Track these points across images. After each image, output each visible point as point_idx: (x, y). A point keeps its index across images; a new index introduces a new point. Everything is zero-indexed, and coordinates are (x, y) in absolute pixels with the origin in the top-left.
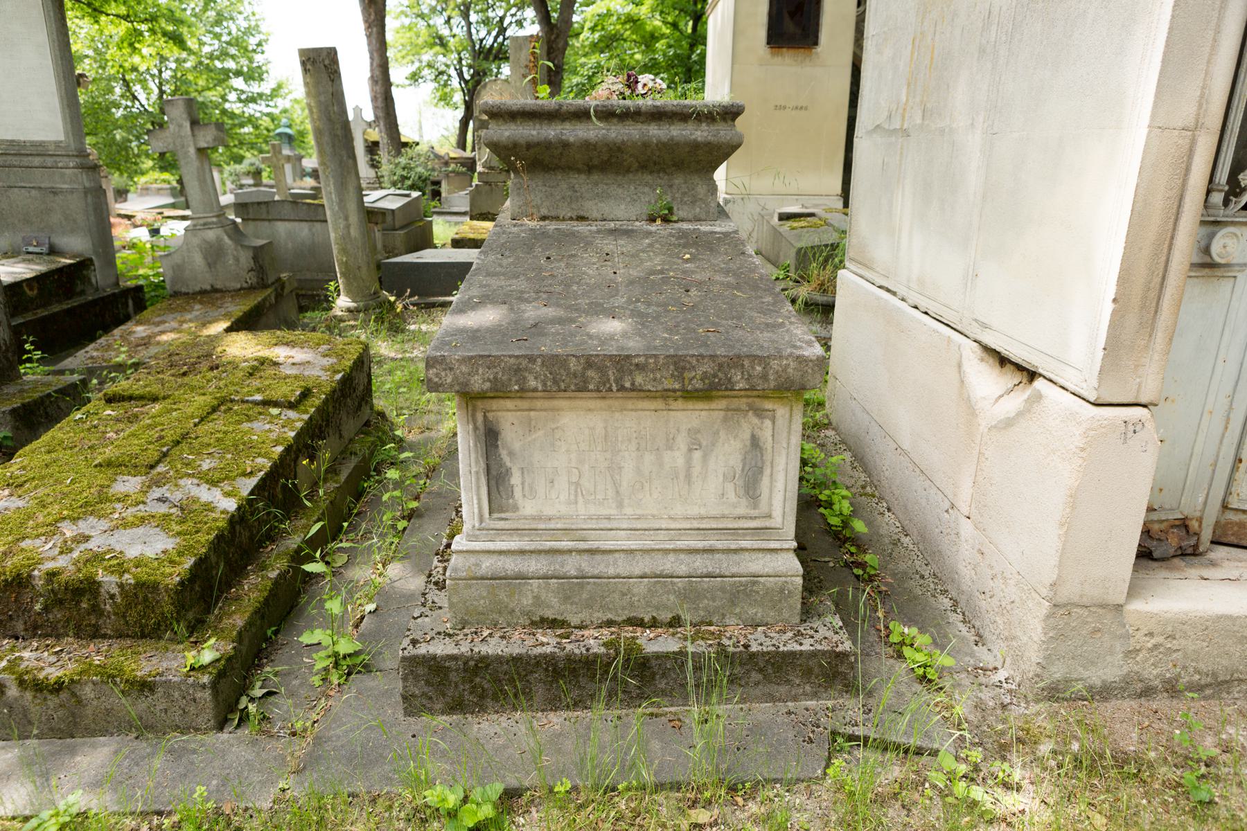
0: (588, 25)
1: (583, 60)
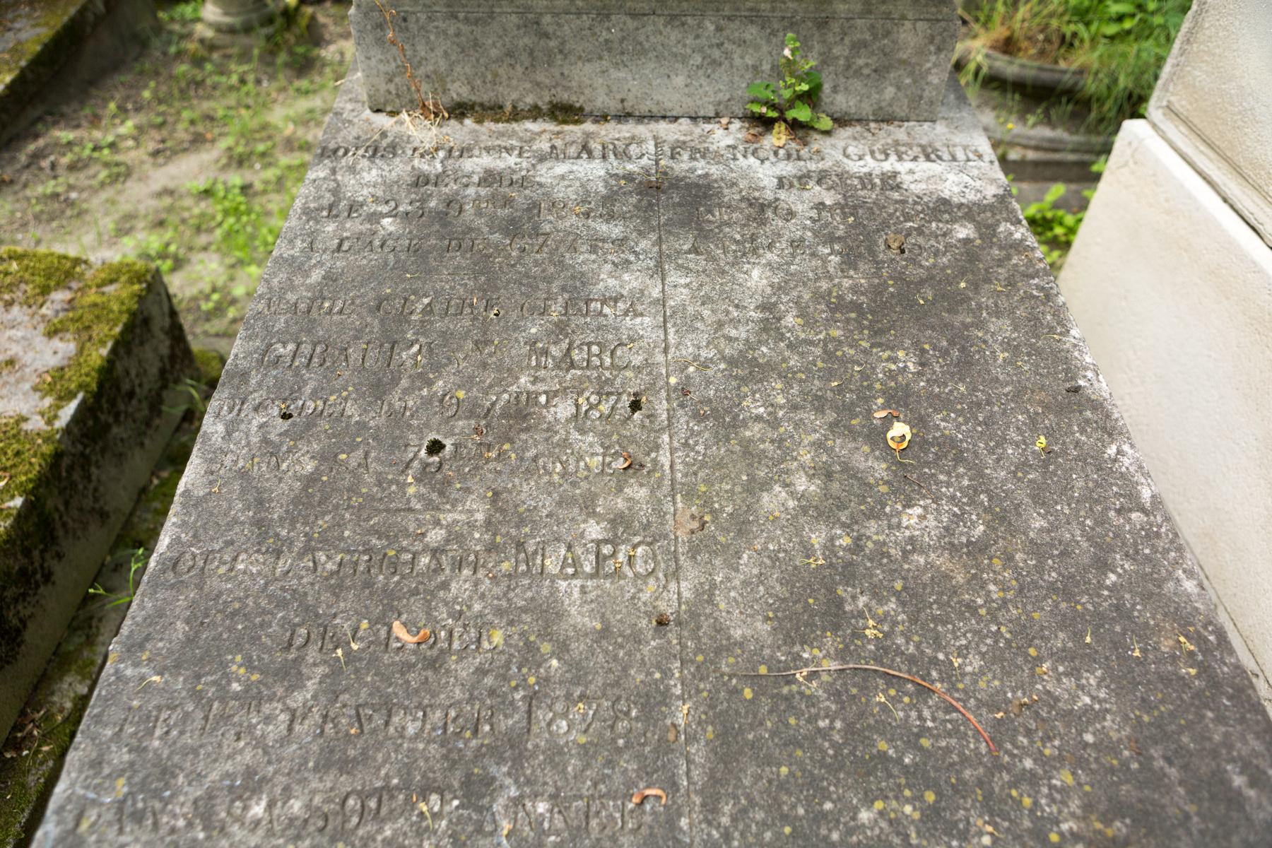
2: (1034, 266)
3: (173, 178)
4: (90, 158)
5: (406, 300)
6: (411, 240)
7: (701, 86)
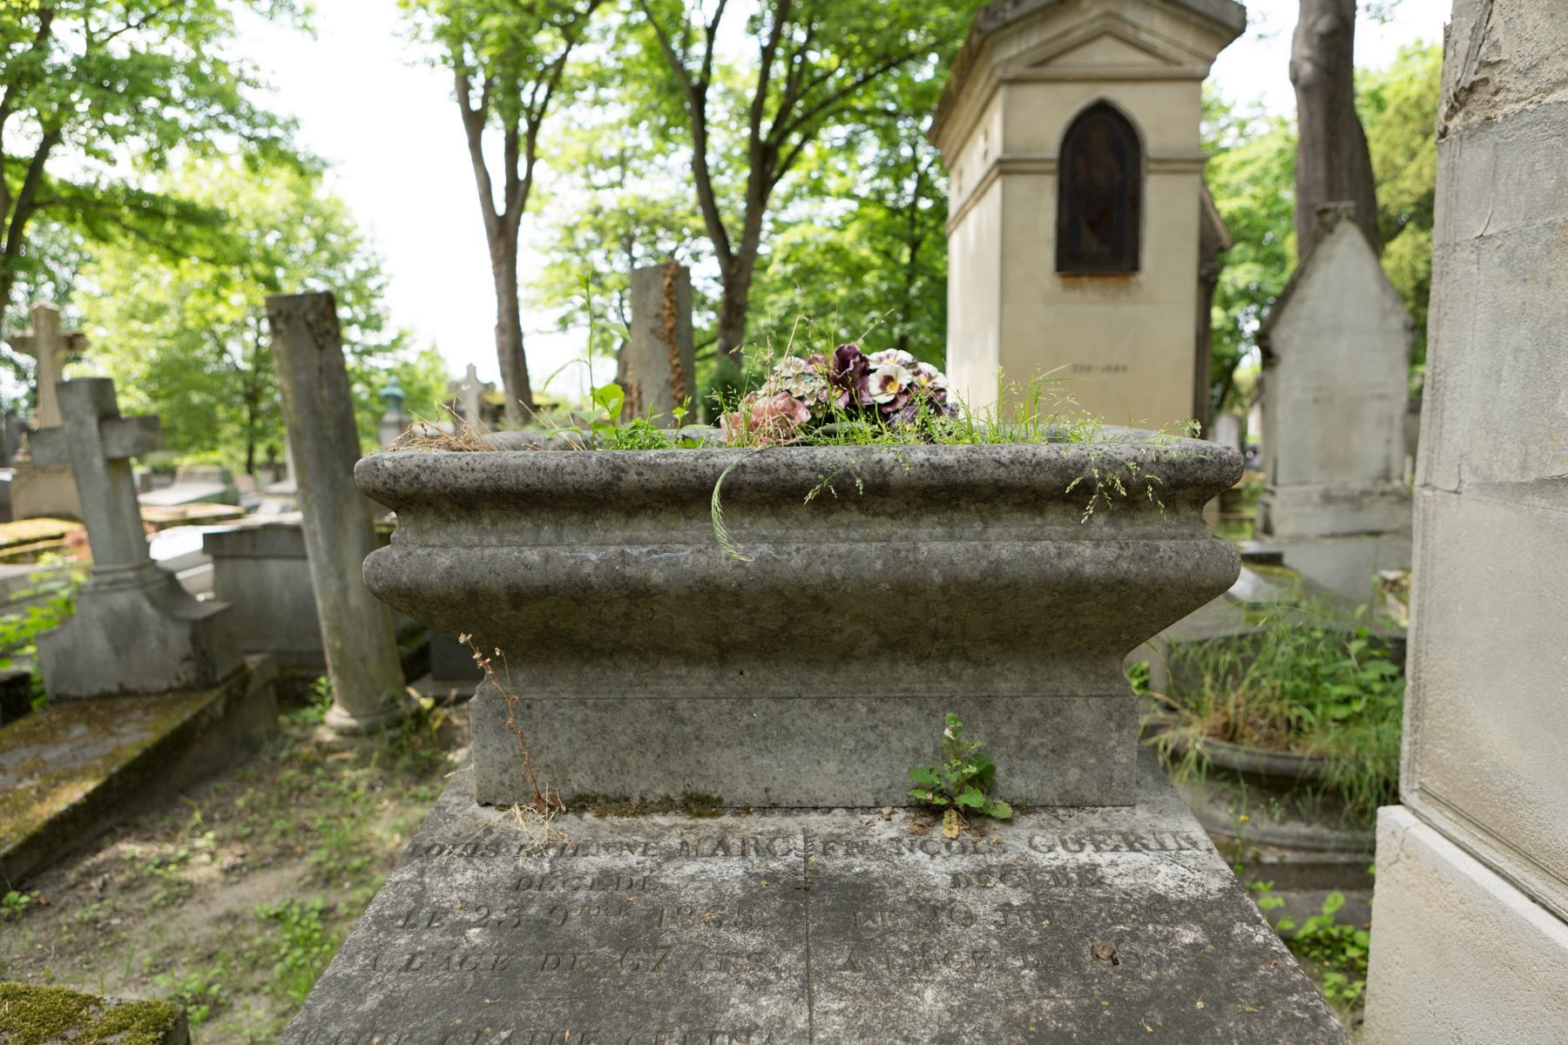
0: (779, 256)
1: (773, 297)
2: (1288, 977)
3: (241, 900)
4: (152, 875)
5: (479, 1033)
6: (499, 955)
7: (856, 772)
